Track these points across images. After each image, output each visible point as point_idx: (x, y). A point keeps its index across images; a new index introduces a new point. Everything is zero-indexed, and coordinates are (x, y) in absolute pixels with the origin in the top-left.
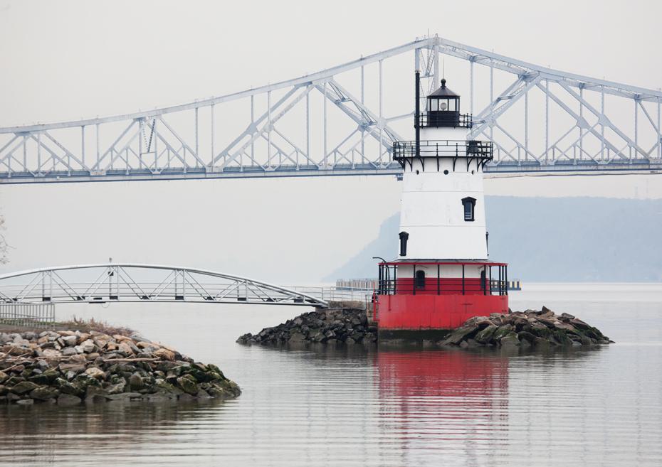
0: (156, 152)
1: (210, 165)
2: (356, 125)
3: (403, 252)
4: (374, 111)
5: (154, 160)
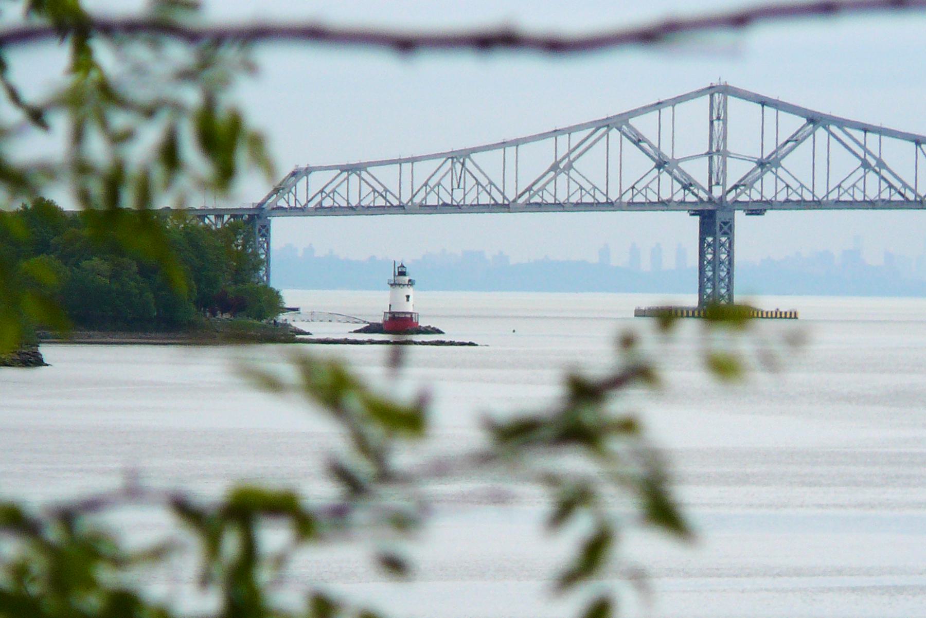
0: (464, 189)
1: (514, 201)
2: (654, 164)
3: (390, 309)
4: (666, 151)
5: (466, 196)
